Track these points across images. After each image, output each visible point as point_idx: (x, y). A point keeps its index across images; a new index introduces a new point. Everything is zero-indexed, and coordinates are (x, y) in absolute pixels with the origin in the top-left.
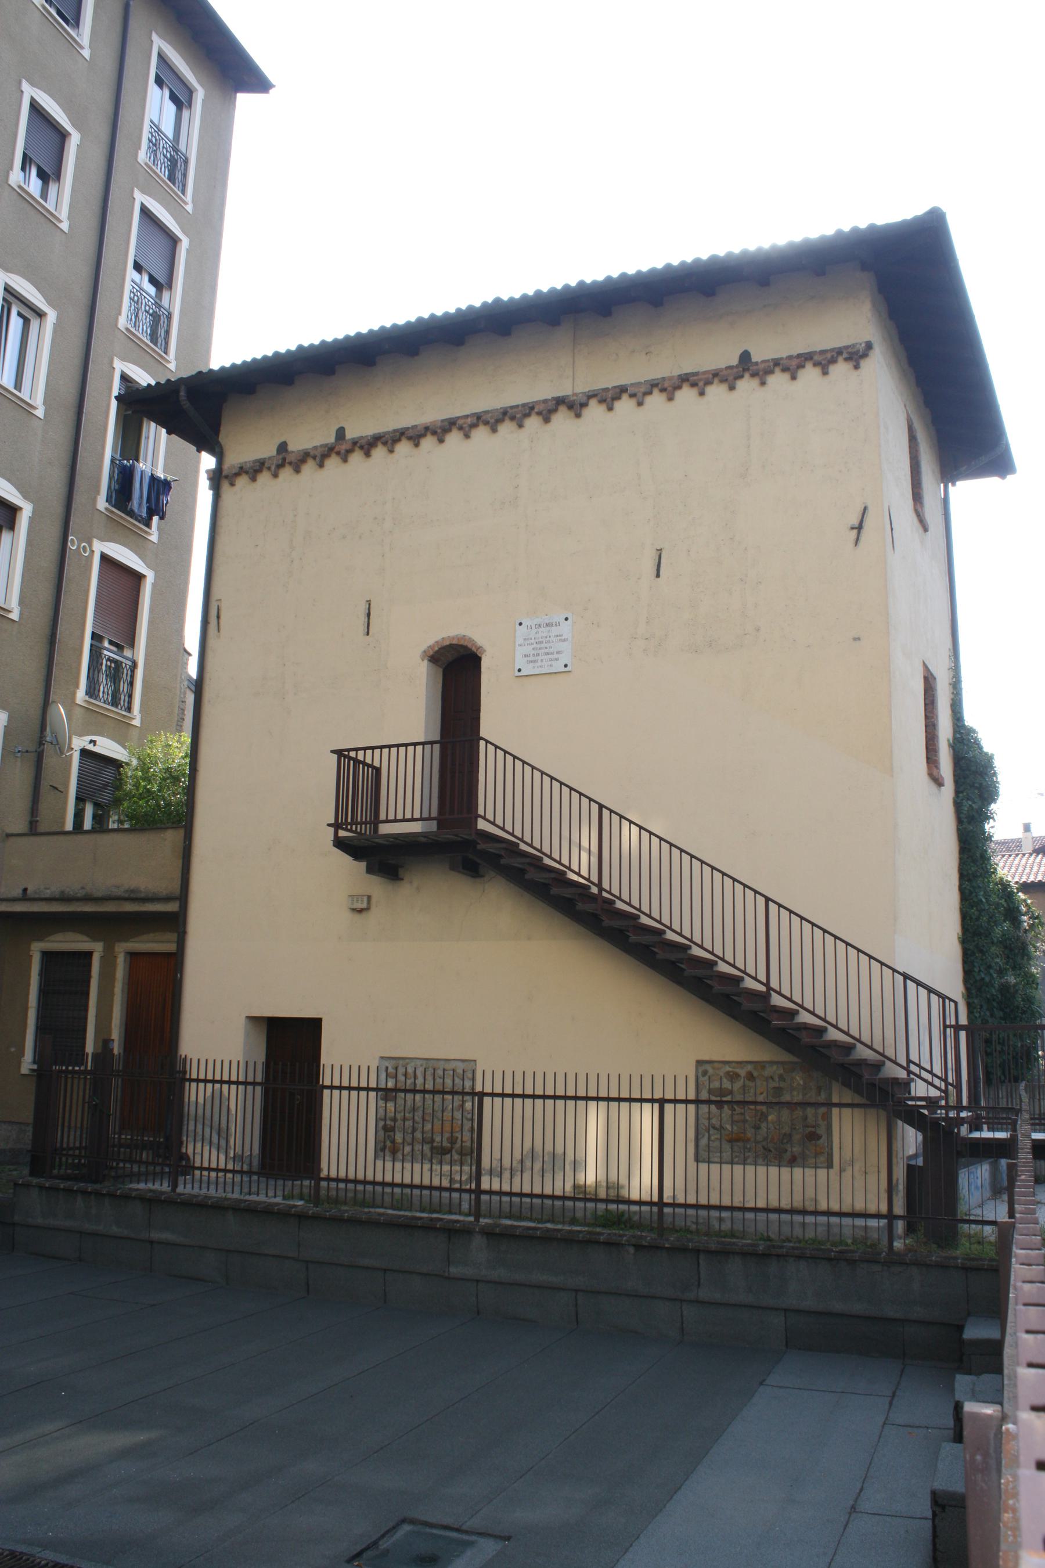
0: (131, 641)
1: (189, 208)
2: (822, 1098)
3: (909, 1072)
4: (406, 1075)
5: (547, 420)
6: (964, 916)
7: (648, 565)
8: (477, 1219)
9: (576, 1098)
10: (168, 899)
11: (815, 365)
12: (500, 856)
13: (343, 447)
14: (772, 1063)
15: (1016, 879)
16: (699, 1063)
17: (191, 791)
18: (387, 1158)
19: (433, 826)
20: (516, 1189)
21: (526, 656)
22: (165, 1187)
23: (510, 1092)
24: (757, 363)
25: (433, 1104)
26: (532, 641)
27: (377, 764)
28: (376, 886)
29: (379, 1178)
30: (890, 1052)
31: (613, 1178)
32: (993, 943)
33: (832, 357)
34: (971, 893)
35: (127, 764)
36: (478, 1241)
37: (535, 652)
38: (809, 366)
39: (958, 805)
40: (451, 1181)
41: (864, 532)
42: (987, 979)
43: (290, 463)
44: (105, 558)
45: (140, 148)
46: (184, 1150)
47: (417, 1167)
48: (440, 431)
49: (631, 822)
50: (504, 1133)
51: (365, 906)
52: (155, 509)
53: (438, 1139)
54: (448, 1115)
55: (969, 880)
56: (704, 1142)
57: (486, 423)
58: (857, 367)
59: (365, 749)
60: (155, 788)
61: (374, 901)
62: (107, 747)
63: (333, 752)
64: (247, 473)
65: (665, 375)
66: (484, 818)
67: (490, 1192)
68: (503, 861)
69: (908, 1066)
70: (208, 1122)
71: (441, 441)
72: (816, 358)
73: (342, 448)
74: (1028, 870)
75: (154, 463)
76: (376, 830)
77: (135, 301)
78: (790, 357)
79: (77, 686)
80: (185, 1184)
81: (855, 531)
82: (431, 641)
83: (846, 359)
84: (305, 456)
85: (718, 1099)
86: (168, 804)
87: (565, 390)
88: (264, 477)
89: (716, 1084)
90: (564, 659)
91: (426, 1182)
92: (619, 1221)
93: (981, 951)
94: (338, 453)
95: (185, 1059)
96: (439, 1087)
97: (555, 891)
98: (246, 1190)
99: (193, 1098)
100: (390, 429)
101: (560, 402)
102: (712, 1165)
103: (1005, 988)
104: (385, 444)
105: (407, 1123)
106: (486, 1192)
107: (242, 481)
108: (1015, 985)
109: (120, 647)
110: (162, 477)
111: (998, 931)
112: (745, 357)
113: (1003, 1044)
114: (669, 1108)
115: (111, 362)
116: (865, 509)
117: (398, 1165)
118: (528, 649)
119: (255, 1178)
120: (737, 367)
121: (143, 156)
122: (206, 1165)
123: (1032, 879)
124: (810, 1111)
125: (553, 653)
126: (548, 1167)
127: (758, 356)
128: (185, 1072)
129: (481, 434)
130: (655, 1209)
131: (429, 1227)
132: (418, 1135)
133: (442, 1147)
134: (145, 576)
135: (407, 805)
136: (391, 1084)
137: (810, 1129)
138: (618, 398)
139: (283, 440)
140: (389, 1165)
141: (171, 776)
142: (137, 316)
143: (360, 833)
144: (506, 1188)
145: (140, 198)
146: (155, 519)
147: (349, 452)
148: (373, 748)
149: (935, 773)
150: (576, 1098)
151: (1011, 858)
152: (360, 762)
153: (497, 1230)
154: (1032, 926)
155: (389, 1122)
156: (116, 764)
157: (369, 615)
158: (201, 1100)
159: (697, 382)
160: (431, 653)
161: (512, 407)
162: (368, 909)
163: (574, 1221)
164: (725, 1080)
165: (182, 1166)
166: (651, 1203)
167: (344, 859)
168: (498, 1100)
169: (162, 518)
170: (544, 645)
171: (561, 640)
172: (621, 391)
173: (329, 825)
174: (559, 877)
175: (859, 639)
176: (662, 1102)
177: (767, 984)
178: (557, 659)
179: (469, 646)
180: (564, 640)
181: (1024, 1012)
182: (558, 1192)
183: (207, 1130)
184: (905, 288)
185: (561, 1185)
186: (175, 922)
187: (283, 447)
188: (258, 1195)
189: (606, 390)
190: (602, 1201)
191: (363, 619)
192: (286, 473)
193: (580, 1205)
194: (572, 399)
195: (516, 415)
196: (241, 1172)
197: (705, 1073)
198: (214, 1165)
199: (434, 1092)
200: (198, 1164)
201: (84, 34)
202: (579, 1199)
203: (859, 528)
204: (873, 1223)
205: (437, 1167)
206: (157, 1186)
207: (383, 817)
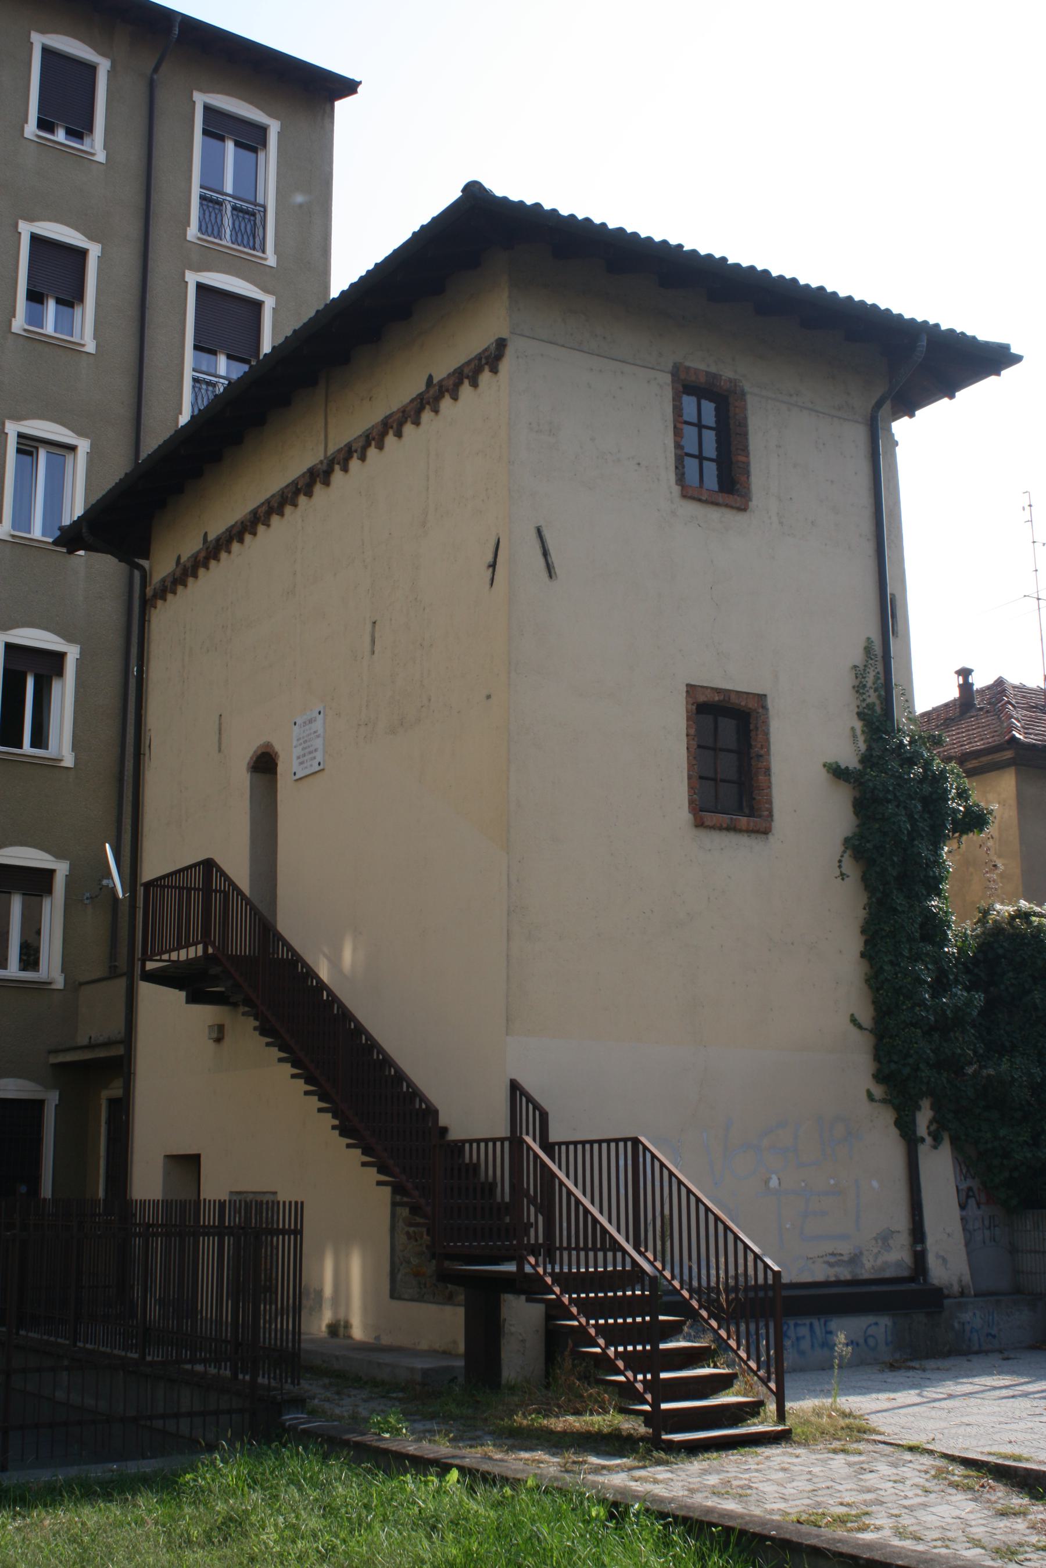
10: (107, 1044)
41: (497, 567)
100: (407, 400)
195: (392, 426)
201: (96, 145)
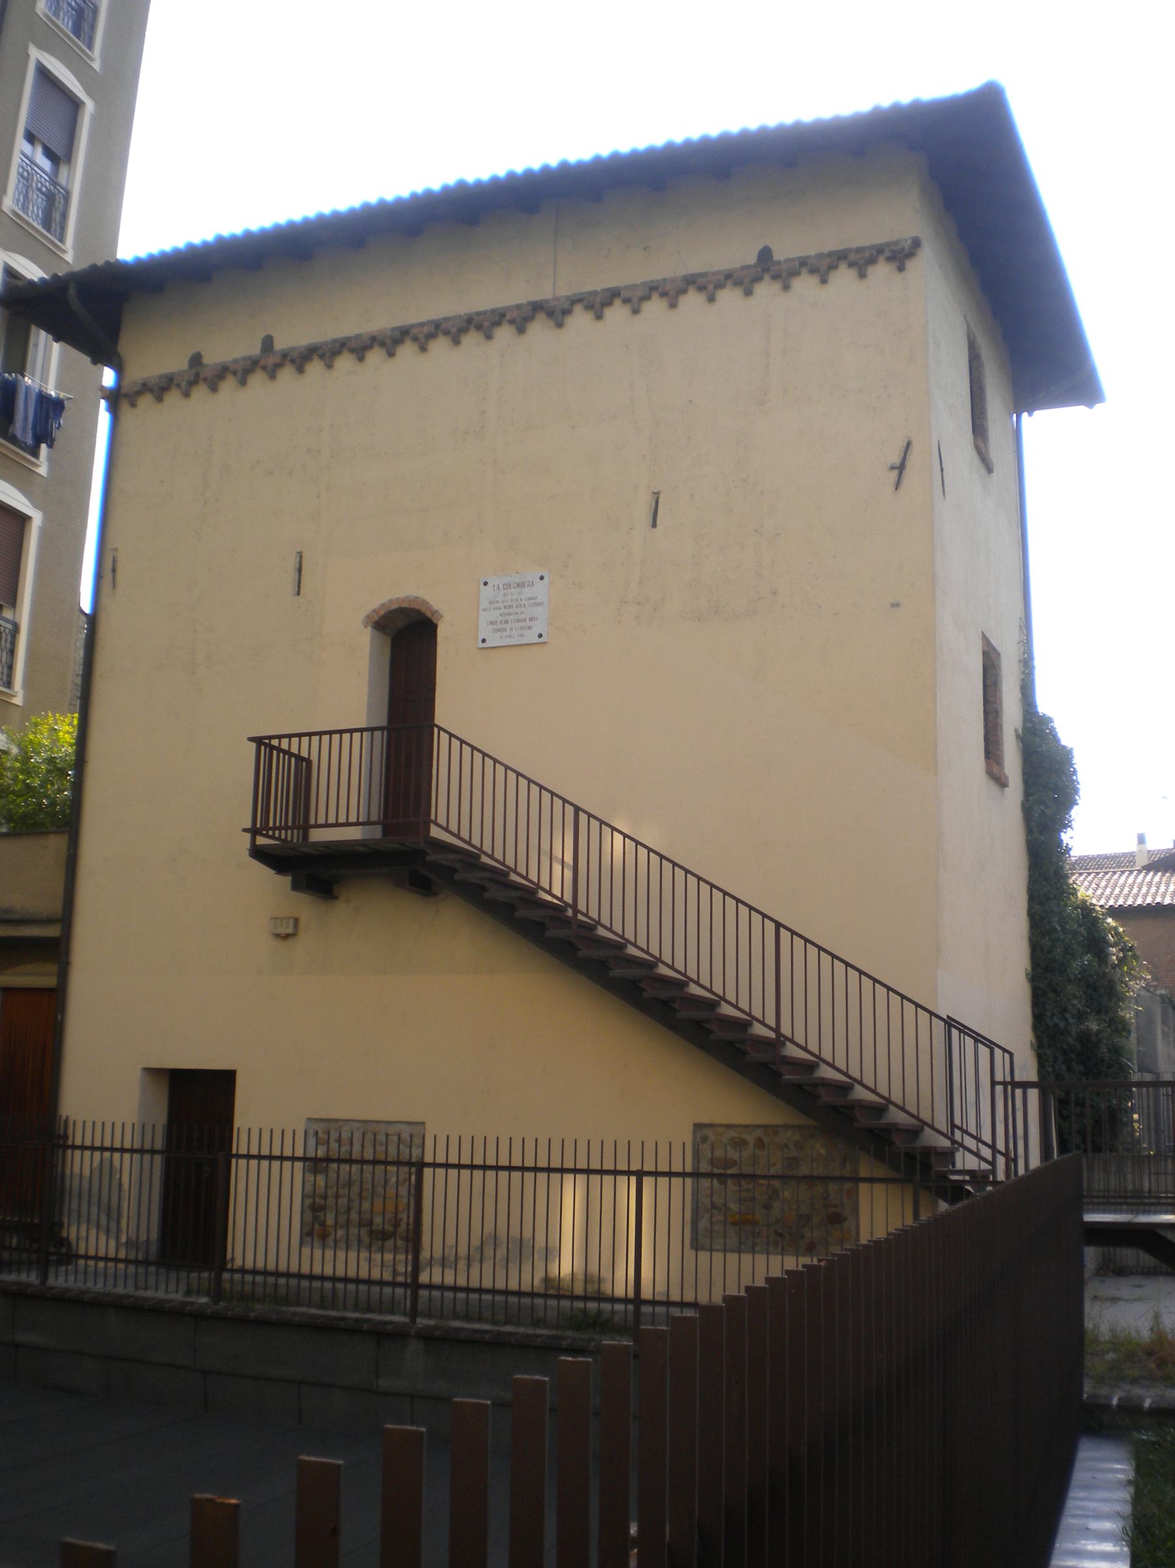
1: (96, 65)
2: (847, 1172)
3: (954, 1142)
4: (339, 1140)
5: (521, 330)
6: (1035, 948)
8: (413, 1321)
9: (549, 1170)
10: (48, 921)
11: (850, 265)
12: (455, 870)
13: (270, 361)
14: (786, 1127)
15: (1102, 902)
16: (698, 1127)
17: (78, 786)
18: (316, 1244)
19: (376, 832)
20: (475, 1283)
21: (492, 623)
22: (31, 1278)
23: (290, 1155)
24: (779, 263)
25: (370, 1177)
27: (304, 754)
28: (304, 906)
29: (305, 1270)
30: (925, 1115)
31: (593, 1268)
32: (1069, 980)
34: (1042, 919)
36: (414, 1347)
39: (1027, 810)
40: (395, 1273)
42: (1062, 1025)
43: (205, 380)
46: (64, 1234)
47: (352, 1255)
48: (390, 342)
49: (613, 829)
50: (452, 1213)
51: (290, 930)
52: (43, 435)
53: (378, 1220)
54: (391, 1192)
55: (1041, 903)
56: (704, 1223)
57: (447, 333)
58: (901, 269)
59: (290, 736)
60: (37, 783)
61: (302, 924)
63: (251, 739)
64: (151, 390)
65: (668, 276)
67: (430, 1287)
68: (457, 876)
69: (953, 1133)
70: (95, 1200)
71: (391, 354)
72: (852, 257)
73: (270, 361)
74: (1153, 889)
75: (44, 378)
76: (306, 836)
77: (26, 178)
78: (820, 256)
80: (66, 1275)
81: (896, 472)
83: (889, 259)
84: (223, 372)
85: (722, 1171)
86: (53, 804)
87: (545, 292)
89: (719, 1153)
90: (538, 628)
91: (364, 1274)
92: (600, 1324)
93: (1055, 991)
94: (264, 368)
95: (66, 1121)
96: (382, 1157)
97: (521, 913)
98: (141, 1283)
99: (77, 1169)
102: (714, 1254)
103: (1085, 1038)
104: (322, 357)
105: (341, 1201)
106: (647, 1302)
107: (146, 401)
108: (1098, 1033)
110: (53, 394)
111: (1076, 966)
112: (765, 255)
113: (1083, 1105)
114: (648, 1182)
116: (909, 444)
117: (329, 1254)
118: (495, 615)
119: (152, 1269)
120: (755, 266)
122: (92, 1252)
123: (1139, 901)
124: (833, 1187)
125: (525, 620)
126: (514, 1254)
128: (66, 1137)
129: (440, 347)
130: (631, 1307)
131: (354, 1330)
132: (354, 1216)
133: (383, 1232)
134: (30, 518)
135: (345, 809)
136: (321, 1153)
137: (832, 1210)
138: (608, 303)
139: (196, 350)
140: (318, 1253)
141: (56, 768)
142: (26, 197)
143: (285, 840)
144: (462, 1282)
146: (44, 446)
147: (278, 366)
148: (300, 735)
149: (995, 769)
150: (549, 1170)
151: (1116, 877)
153: (437, 1333)
154: (1122, 961)
155: (317, 1200)
157: (300, 570)
158: (87, 1172)
159: (708, 285)
160: (376, 618)
161: (478, 314)
162: (293, 935)
163: (537, 1323)
164: (729, 1148)
165: (68, 1256)
166: (625, 1301)
167: (263, 873)
168: (441, 1172)
169: (50, 446)
170: (514, 610)
172: (612, 296)
173: (245, 830)
174: (528, 895)
175: (898, 605)
176: (640, 1175)
177: (777, 1030)
178: (530, 628)
179: (423, 610)
180: (539, 604)
181: (1110, 1066)
182: (526, 1287)
183: (94, 1211)
185: (528, 1278)
186: (56, 950)
187: (196, 360)
188: (177, 1291)
189: (594, 294)
190: (578, 1298)
193: (552, 1303)
194: (552, 304)
195: (484, 324)
196: (137, 1262)
197: (704, 1139)
198: (102, 1253)
199: (375, 1162)
200: (82, 1251)
202: (552, 1296)
203: (901, 468)
204: (620, 1307)
205: (377, 1257)
206: (23, 1277)
207: (312, 822)
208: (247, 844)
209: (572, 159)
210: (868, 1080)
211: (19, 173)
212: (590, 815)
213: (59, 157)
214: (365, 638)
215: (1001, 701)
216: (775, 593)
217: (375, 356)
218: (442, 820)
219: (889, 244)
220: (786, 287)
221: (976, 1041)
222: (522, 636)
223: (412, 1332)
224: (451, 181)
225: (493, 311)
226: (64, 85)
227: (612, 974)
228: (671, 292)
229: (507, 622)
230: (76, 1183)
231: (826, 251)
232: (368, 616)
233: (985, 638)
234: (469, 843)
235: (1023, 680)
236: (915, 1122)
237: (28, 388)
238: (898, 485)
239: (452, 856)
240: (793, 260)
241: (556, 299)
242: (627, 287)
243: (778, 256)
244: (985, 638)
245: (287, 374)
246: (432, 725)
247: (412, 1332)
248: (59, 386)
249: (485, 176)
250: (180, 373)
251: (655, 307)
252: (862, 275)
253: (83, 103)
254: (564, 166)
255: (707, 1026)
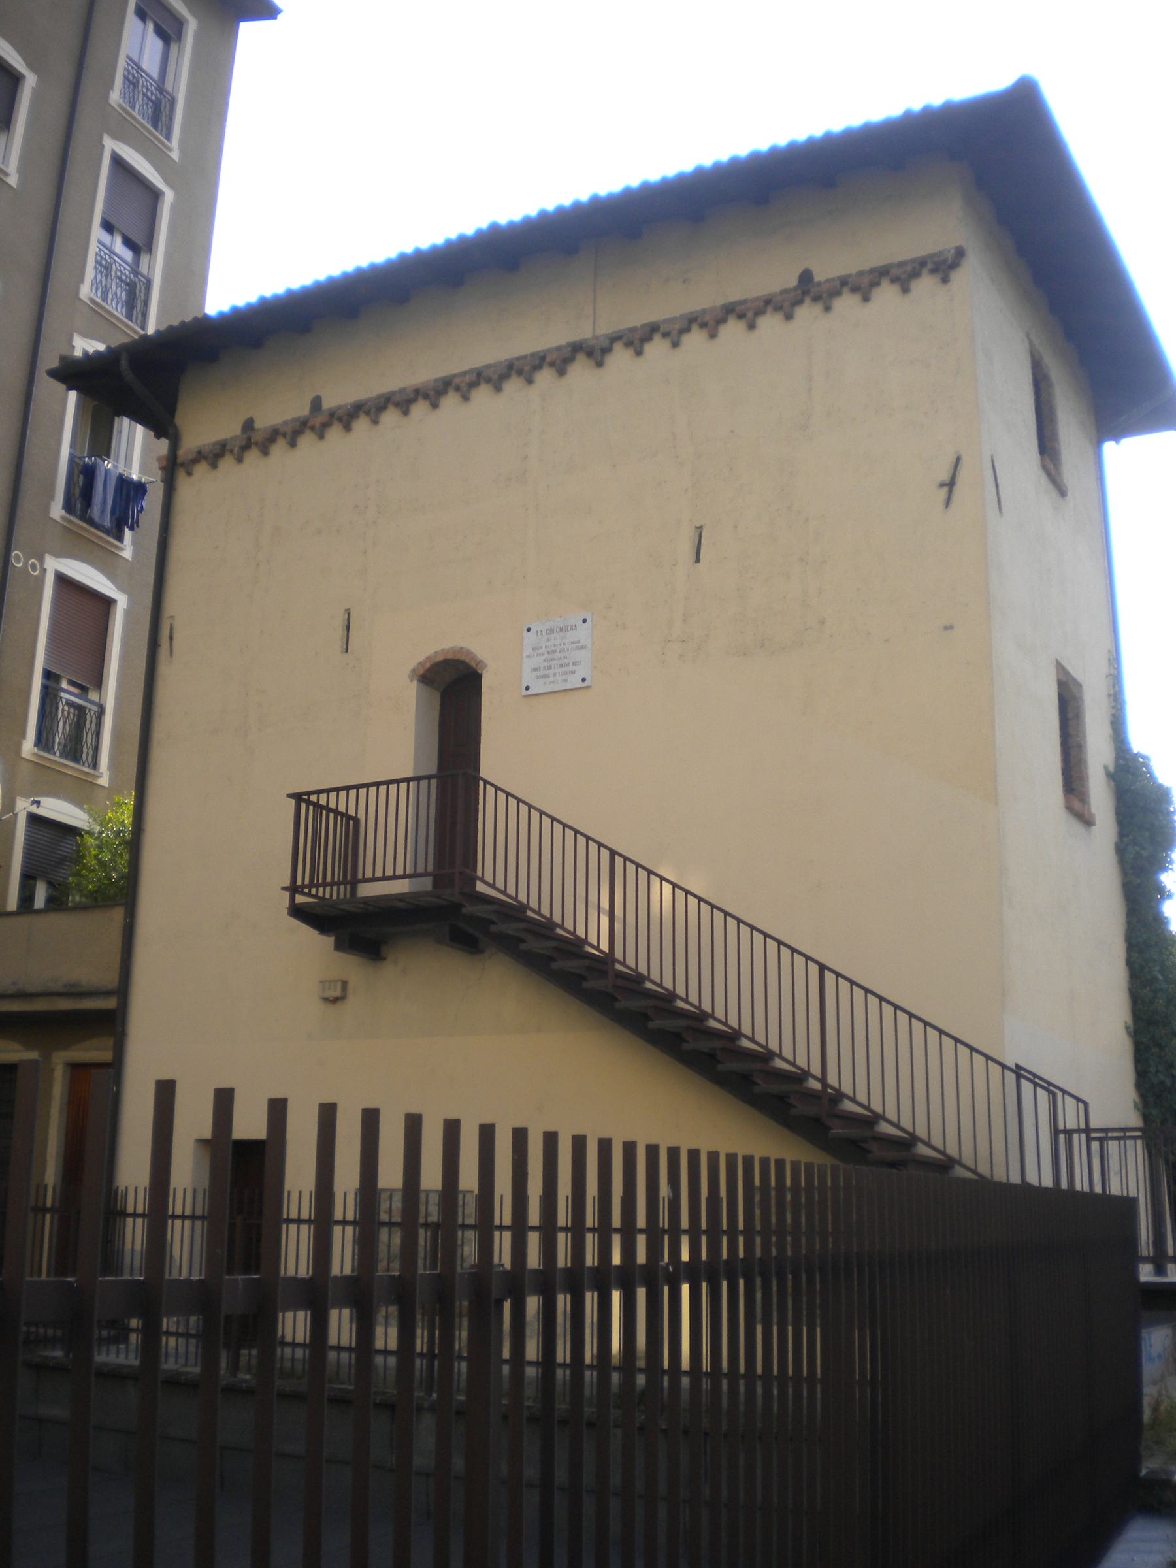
0: (98, 680)
1: (175, 155)
5: (562, 372)
7: (685, 548)
10: (108, 994)
21: (535, 670)
24: (819, 284)
26: (544, 650)
27: (352, 812)
28: (350, 966)
33: (914, 268)
35: (88, 832)
37: (546, 664)
38: (885, 285)
41: (957, 489)
43: (256, 444)
44: (63, 581)
45: (112, 88)
48: (433, 394)
49: (662, 879)
51: (338, 993)
57: (488, 380)
59: (328, 791)
61: (350, 987)
62: (57, 809)
63: (290, 796)
64: (205, 458)
66: (482, 880)
68: (493, 929)
72: (895, 272)
73: (321, 421)
77: (104, 267)
78: (861, 274)
79: (23, 735)
81: (946, 489)
82: (421, 658)
84: (274, 435)
87: (583, 332)
88: (227, 463)
90: (581, 672)
93: (1159, 1045)
94: (312, 428)
99: (128, 1246)
100: (374, 394)
101: (577, 348)
104: (368, 413)
107: (201, 469)
109: (84, 689)
112: (806, 277)
115: (70, 340)
116: (958, 459)
118: (538, 661)
120: (795, 289)
121: (115, 97)
125: (568, 665)
127: (821, 275)
129: (483, 394)
143: (324, 898)
145: (110, 145)
147: (326, 425)
148: (338, 790)
149: (1077, 805)
152: (322, 807)
156: (70, 831)
159: (746, 313)
161: (518, 359)
167: (306, 934)
169: (131, 528)
170: (558, 655)
171: (578, 648)
173: (284, 889)
174: (574, 947)
180: (582, 648)
184: (996, 172)
187: (249, 425)
189: (633, 330)
191: (340, 632)
192: (252, 456)
195: (524, 369)
203: (950, 484)
208: (286, 903)
209: (603, 192)
210: (891, 1114)
211: (96, 261)
212: (626, 859)
213: (140, 246)
214: (411, 691)
215: (1084, 736)
216: (822, 622)
217: (420, 409)
218: (488, 877)
219: (932, 256)
220: (828, 309)
221: (1036, 1085)
222: (566, 681)
223: (426, 1405)
224: (484, 225)
225: (533, 355)
226: (145, 178)
227: (685, 1046)
228: (710, 322)
229: (550, 667)
230: (127, 1259)
231: (867, 268)
232: (414, 670)
233: (1059, 666)
234: (504, 893)
235: (1113, 715)
236: (940, 1157)
237: (107, 471)
238: (948, 502)
239: (489, 907)
240: (833, 279)
241: (595, 337)
242: (666, 321)
243: (818, 277)
244: (1059, 666)
245: (335, 433)
246: (478, 778)
247: (426, 1405)
248: (143, 469)
249: (517, 217)
250: (234, 438)
251: (695, 339)
252: (905, 290)
253: (163, 193)
254: (595, 200)
255: (864, 1145)
